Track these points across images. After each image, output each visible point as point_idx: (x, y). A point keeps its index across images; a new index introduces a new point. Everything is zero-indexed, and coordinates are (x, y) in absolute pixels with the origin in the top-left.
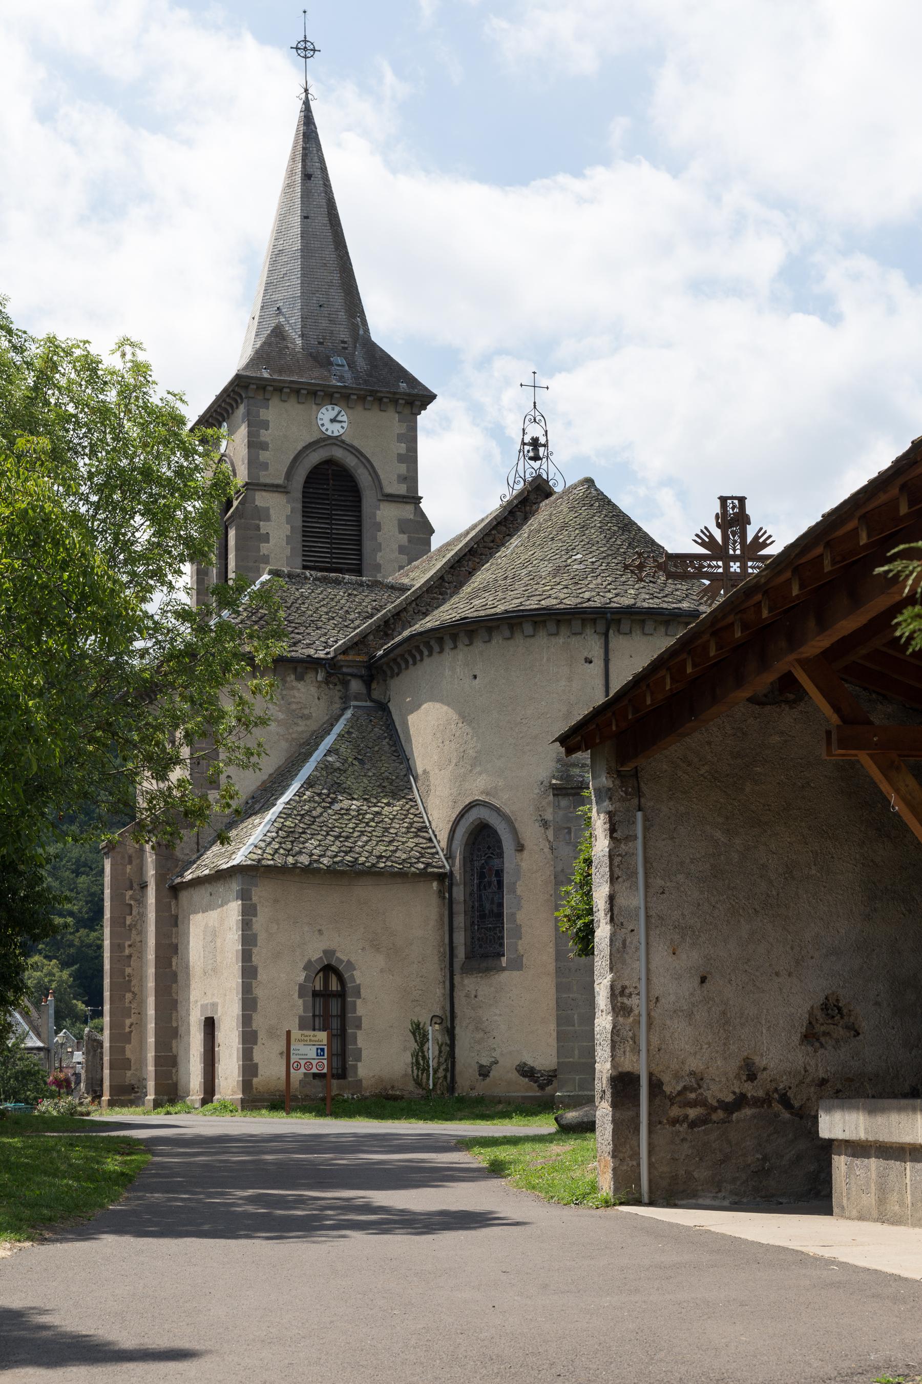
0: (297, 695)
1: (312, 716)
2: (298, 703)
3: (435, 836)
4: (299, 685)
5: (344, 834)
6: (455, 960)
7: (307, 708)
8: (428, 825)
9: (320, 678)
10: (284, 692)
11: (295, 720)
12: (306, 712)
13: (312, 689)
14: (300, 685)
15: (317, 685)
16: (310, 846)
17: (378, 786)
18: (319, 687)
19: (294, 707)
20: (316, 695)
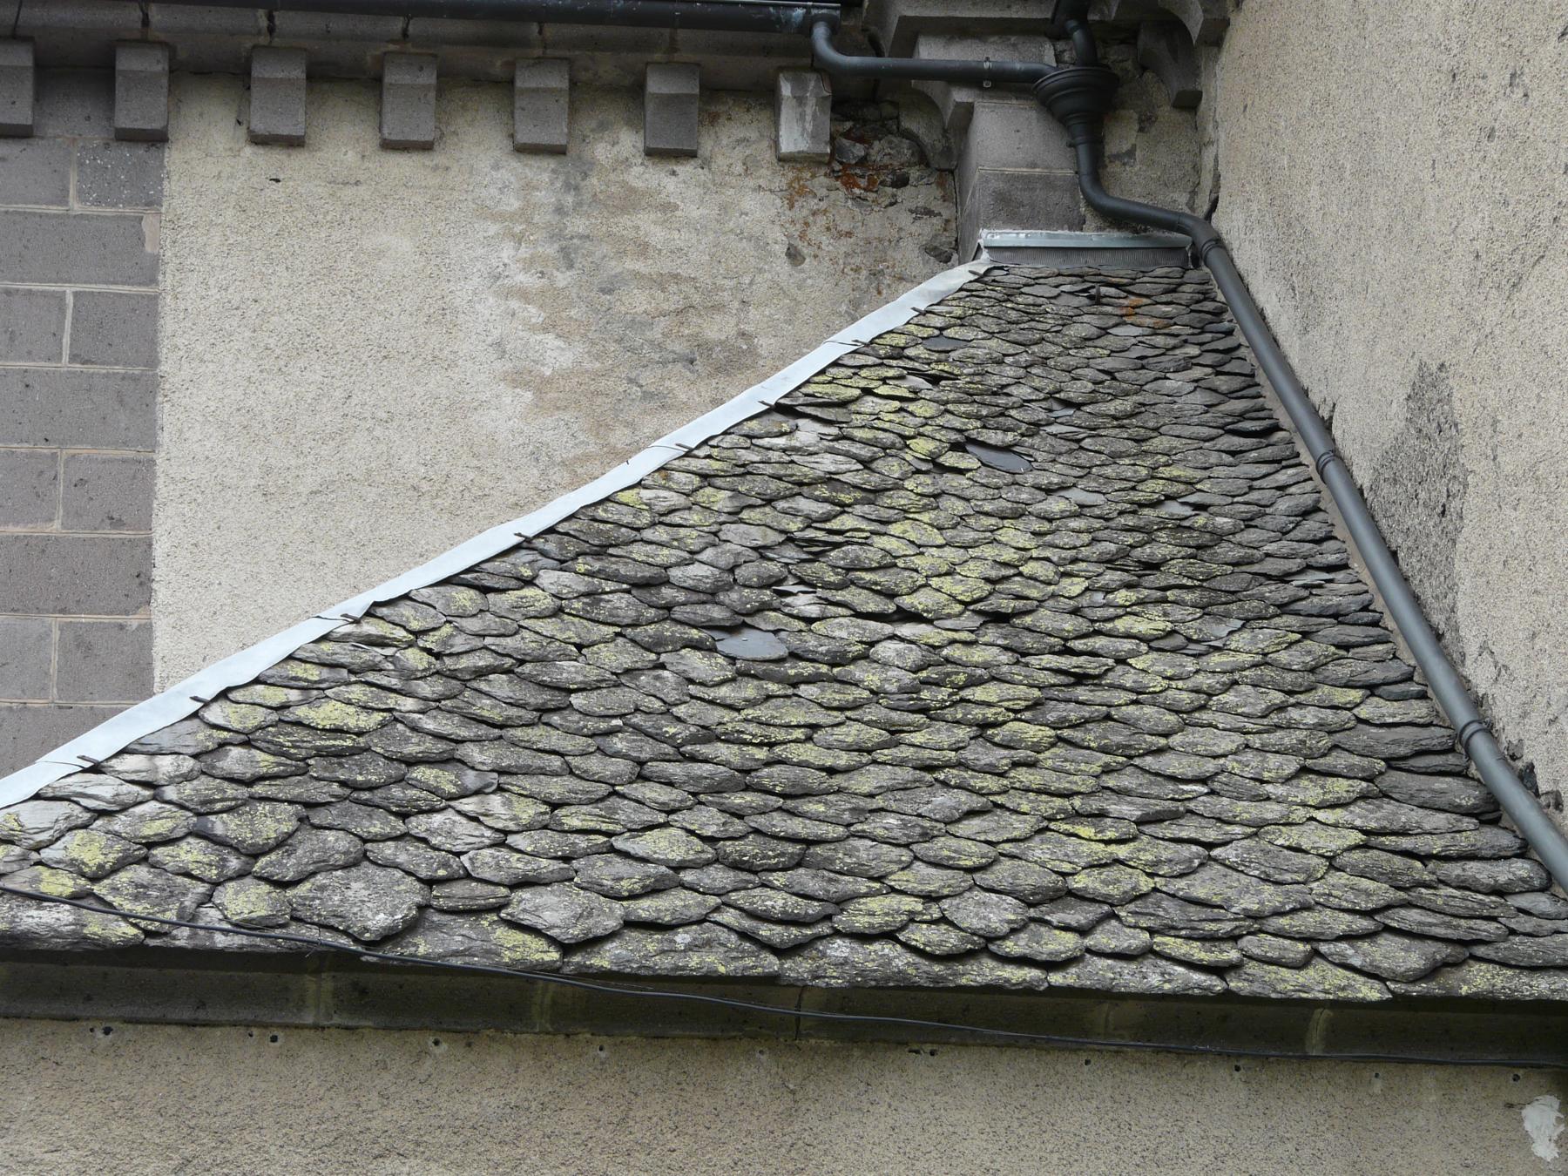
0: (658, 236)
1: (752, 351)
2: (660, 282)
3: (1526, 777)
4: (671, 184)
5: (775, 776)
6: (1362, 979)
7: (718, 308)
8: (1462, 715)
9: (793, 138)
10: (578, 225)
11: (648, 378)
12: (717, 329)
13: (750, 202)
14: (675, 182)
15: (780, 182)
16: (465, 827)
17: (1109, 562)
18: (793, 195)
19: (638, 301)
20: (778, 241)
